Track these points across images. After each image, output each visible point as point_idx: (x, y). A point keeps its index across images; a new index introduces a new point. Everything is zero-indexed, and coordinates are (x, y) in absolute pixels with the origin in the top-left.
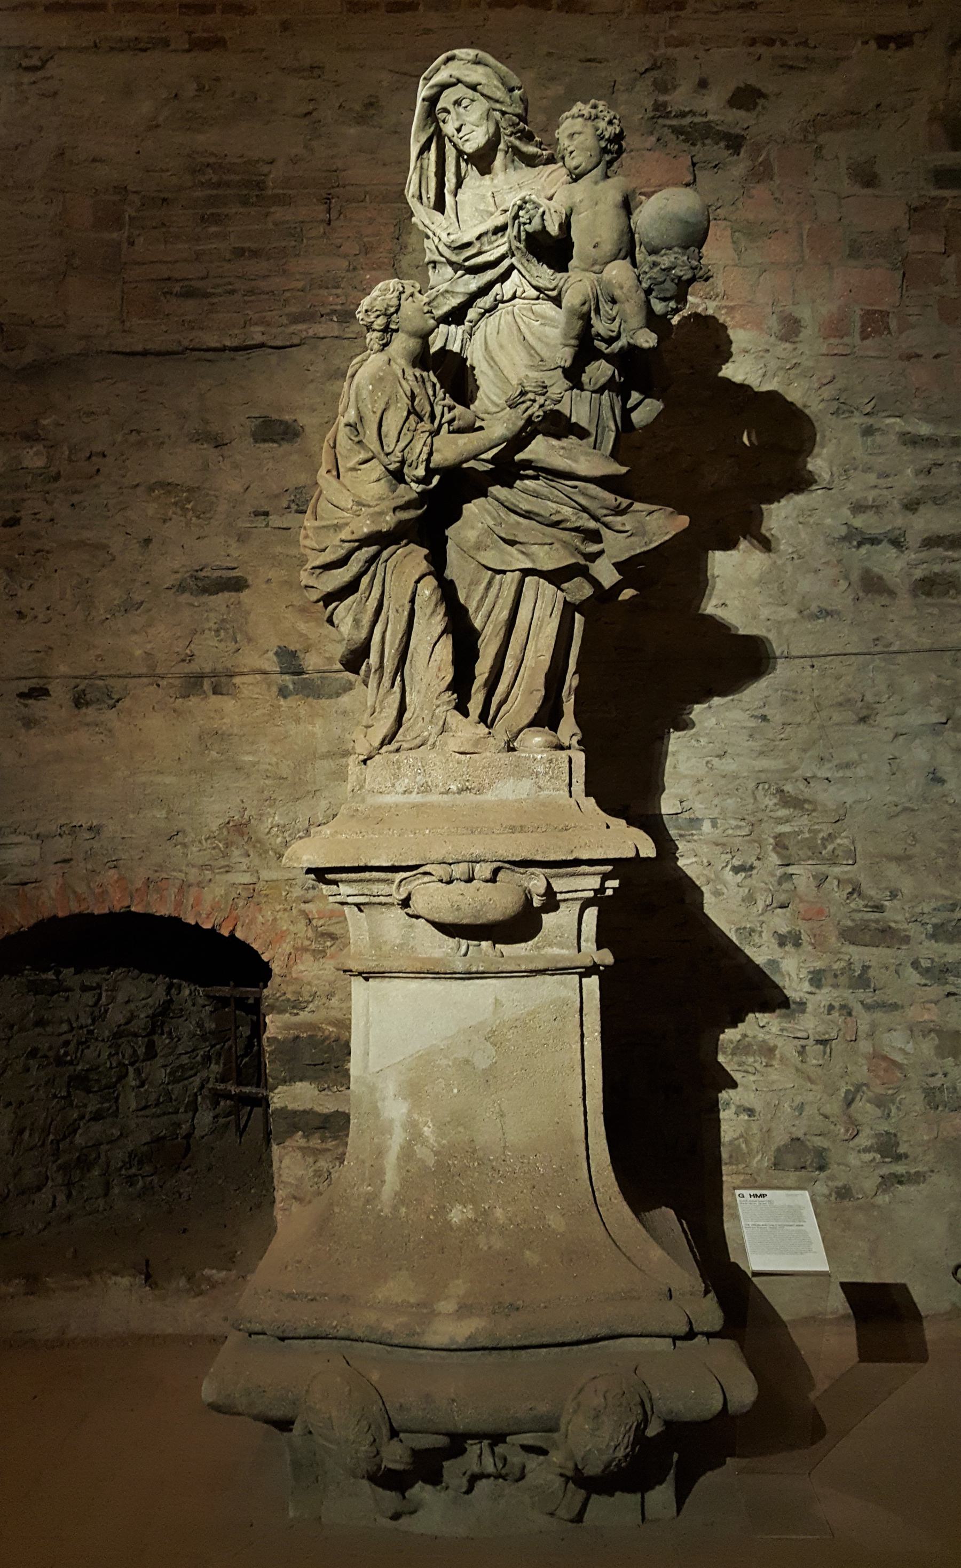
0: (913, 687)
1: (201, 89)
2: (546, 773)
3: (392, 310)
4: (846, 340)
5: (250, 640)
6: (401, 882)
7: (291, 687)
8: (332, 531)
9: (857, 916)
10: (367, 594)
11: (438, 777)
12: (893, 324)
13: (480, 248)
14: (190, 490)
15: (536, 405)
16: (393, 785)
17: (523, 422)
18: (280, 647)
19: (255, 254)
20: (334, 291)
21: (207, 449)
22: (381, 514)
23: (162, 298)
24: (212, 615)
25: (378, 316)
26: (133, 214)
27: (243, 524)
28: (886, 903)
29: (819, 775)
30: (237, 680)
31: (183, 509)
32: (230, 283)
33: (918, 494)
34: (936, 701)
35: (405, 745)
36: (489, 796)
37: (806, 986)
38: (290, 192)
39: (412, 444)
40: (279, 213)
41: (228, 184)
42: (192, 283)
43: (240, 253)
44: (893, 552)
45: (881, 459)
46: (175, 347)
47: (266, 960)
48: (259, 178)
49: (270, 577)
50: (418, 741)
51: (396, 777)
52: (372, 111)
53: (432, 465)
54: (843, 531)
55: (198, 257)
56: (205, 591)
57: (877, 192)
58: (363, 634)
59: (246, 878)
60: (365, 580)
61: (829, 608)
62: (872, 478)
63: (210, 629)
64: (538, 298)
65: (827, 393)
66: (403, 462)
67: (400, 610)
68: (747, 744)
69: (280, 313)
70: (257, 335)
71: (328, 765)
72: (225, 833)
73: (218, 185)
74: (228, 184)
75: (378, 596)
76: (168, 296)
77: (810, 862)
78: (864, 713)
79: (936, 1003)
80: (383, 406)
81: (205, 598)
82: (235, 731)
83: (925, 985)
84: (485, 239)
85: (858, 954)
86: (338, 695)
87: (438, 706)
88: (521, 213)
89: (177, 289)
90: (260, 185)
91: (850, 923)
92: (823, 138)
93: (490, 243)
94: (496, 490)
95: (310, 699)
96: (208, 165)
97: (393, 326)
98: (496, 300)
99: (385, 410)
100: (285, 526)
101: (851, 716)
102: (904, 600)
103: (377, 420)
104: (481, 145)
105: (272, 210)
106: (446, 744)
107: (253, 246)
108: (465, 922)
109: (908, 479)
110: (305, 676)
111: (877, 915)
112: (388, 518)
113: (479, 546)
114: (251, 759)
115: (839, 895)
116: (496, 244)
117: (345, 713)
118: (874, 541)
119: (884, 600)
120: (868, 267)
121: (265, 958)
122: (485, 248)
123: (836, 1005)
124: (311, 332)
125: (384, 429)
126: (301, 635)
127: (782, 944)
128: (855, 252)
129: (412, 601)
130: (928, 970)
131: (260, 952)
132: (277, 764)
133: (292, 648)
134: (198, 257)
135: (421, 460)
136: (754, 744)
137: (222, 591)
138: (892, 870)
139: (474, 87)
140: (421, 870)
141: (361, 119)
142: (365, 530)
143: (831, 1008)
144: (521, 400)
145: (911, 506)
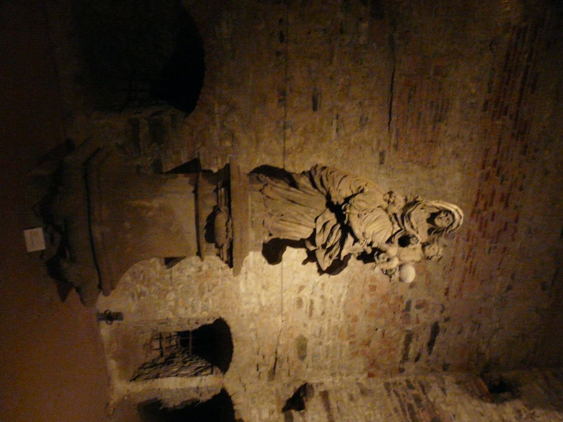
0: (272, 298)
11: (257, 215)
19: (419, 118)
22: (336, 198)
30: (283, 108)
41: (441, 111)
44: (310, 292)
65: (356, 278)
70: (394, 118)
71: (254, 137)
74: (441, 111)
92: (425, 276)
94: (339, 226)
101: (265, 284)
102: (297, 296)
109: (329, 296)
113: (324, 218)
119: (297, 291)
130: (193, 303)
138: (221, 294)
139: (452, 224)
141: (454, 153)
145: (322, 297)
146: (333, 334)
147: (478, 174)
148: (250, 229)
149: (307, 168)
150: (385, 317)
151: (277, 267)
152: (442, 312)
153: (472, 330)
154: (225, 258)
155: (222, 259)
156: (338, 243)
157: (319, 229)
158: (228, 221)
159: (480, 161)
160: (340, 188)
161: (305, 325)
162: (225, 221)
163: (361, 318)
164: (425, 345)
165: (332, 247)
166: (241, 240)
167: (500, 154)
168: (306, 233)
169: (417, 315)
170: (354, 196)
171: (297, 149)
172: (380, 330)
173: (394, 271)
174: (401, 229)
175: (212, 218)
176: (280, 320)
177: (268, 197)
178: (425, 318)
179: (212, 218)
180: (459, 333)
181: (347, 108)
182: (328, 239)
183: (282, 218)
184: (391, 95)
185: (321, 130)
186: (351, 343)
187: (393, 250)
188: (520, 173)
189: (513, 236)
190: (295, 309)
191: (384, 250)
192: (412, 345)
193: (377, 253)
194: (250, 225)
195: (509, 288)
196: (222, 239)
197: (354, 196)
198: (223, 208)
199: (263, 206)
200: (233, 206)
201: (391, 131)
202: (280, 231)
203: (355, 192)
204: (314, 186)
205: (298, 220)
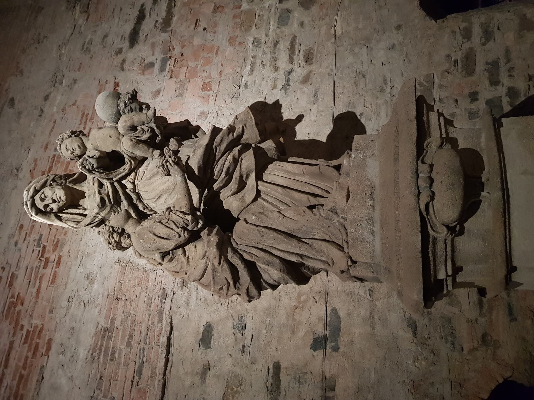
0: (350, 59)
1: (63, 353)
2: (364, 152)
3: (111, 229)
4: (211, 96)
5: (306, 365)
6: (434, 231)
7: (333, 344)
8: (216, 274)
9: (460, 70)
10: (253, 256)
11: (363, 212)
12: (208, 80)
13: (105, 194)
14: (227, 387)
15: (169, 159)
16: (369, 243)
17: (176, 166)
18: (311, 348)
19: (131, 336)
20: (153, 300)
21: (210, 373)
23: (139, 386)
24: (291, 385)
25: (113, 237)
26: (102, 395)
27: (247, 360)
28: (453, 59)
29: (389, 91)
30: (328, 375)
31: (237, 392)
32: (140, 350)
33: (272, 67)
34: (357, 50)
35: (345, 237)
36: (377, 182)
37: (499, 88)
38: (111, 317)
39: (175, 222)
40: (117, 323)
41: (101, 345)
42: (136, 369)
43: (129, 344)
44: (294, 74)
45: (257, 81)
46: (161, 383)
47: (503, 380)
48: (102, 331)
49: (275, 349)
50: (342, 230)
51: (363, 240)
52: (90, 277)
53: (189, 212)
54: (283, 91)
55: (126, 364)
56: (278, 387)
57: (163, 89)
58: (277, 261)
59: (448, 386)
60: (246, 256)
61: (314, 93)
62: (264, 83)
63: (299, 388)
64: (136, 173)
65: (229, 101)
66: (185, 229)
67: (262, 234)
68: (373, 122)
69: (156, 327)
72: (418, 396)
73: (100, 350)
74: (101, 345)
75: (255, 250)
76: (139, 383)
77: (433, 91)
78: (361, 76)
79: (503, 34)
80: (152, 235)
81: (282, 387)
82: (356, 380)
83: (494, 39)
84: (102, 192)
85: (480, 67)
86: (339, 317)
87: (320, 215)
88: (87, 168)
89: (136, 377)
90: (106, 330)
91: (464, 72)
93: (105, 190)
94: (216, 186)
95: (340, 334)
96: (92, 354)
97: (120, 230)
98: (133, 192)
99: (155, 234)
100: (251, 337)
102: (314, 67)
103: (159, 239)
104: (64, 192)
105: (116, 326)
106: (342, 209)
107: (127, 337)
108: (462, 182)
109: (267, 71)
110: (328, 336)
111: (459, 62)
112: (212, 239)
113: (242, 200)
114: (373, 373)
115: (450, 78)
116: (106, 188)
117: (349, 315)
118: (288, 81)
119: (312, 74)
120: (187, 90)
121: (501, 381)
122: (106, 192)
123: (508, 74)
124: (167, 313)
125: (165, 236)
126: (306, 334)
127: (477, 100)
128: (181, 95)
129: (257, 226)
131: (497, 384)
132: (376, 357)
133: (312, 341)
134: (126, 364)
135: (183, 217)
136: (373, 118)
137: (279, 377)
139: (36, 191)
140: (424, 213)
141: (92, 282)
142: (215, 250)
143: (510, 76)
144: (166, 167)
145: (276, 69)
146: (263, 15)
147: (65, 249)
148: (377, 182)
149: (267, 293)
150: (193, 46)
151: (341, 109)
152: (124, 61)
153: (91, 42)
154: (433, 116)
155: (440, 114)
156: (218, 155)
157: (252, 180)
158: (427, 206)
159: (62, 267)
160: (204, 261)
161: (302, 24)
162: (437, 204)
163: (225, 42)
164: (148, 16)
165: (229, 148)
166: (396, 159)
167: (39, 276)
168: (276, 172)
169: (153, 55)
170: (181, 246)
171: (306, 301)
172: (201, 29)
173: (126, 110)
174: (119, 181)
175: (470, 206)
176: (339, 28)
177: (340, 248)
178: (143, 51)
179: (470, 206)
180: (106, 36)
181: (229, 362)
182: (235, 161)
183: (313, 201)
184: (166, 377)
185: (270, 328)
186: (240, 7)
187: (125, 147)
188: (20, 250)
189: (36, 165)
190: (316, 48)
191: (142, 145)
192: (164, 14)
193: (158, 140)
194: (377, 193)
195: (46, 98)
196: (442, 160)
197: (181, 246)
198: (441, 234)
199: (350, 230)
200: (418, 238)
201: (169, 321)
202: (321, 175)
203: (180, 251)
204: (251, 266)
205: (288, 196)
